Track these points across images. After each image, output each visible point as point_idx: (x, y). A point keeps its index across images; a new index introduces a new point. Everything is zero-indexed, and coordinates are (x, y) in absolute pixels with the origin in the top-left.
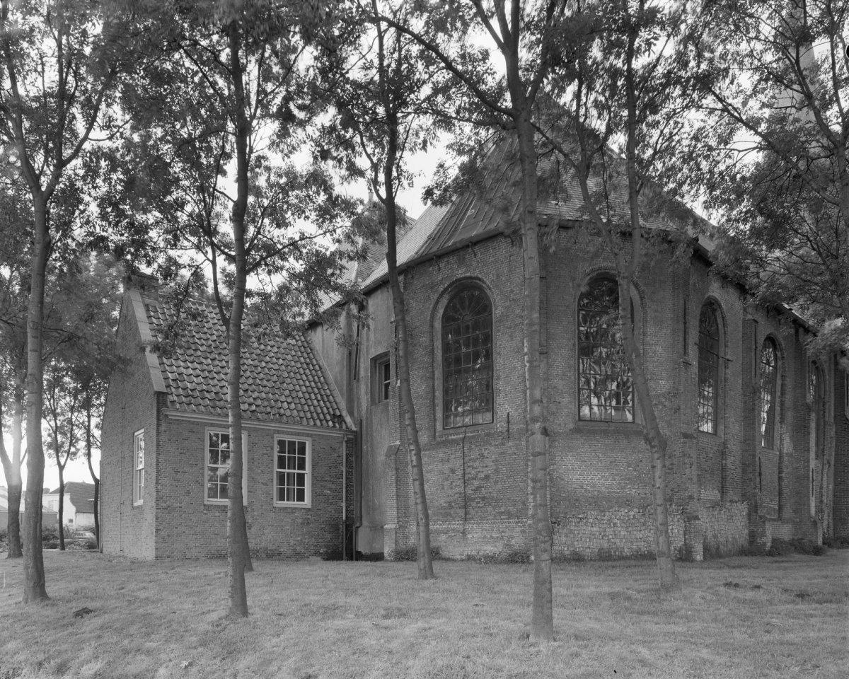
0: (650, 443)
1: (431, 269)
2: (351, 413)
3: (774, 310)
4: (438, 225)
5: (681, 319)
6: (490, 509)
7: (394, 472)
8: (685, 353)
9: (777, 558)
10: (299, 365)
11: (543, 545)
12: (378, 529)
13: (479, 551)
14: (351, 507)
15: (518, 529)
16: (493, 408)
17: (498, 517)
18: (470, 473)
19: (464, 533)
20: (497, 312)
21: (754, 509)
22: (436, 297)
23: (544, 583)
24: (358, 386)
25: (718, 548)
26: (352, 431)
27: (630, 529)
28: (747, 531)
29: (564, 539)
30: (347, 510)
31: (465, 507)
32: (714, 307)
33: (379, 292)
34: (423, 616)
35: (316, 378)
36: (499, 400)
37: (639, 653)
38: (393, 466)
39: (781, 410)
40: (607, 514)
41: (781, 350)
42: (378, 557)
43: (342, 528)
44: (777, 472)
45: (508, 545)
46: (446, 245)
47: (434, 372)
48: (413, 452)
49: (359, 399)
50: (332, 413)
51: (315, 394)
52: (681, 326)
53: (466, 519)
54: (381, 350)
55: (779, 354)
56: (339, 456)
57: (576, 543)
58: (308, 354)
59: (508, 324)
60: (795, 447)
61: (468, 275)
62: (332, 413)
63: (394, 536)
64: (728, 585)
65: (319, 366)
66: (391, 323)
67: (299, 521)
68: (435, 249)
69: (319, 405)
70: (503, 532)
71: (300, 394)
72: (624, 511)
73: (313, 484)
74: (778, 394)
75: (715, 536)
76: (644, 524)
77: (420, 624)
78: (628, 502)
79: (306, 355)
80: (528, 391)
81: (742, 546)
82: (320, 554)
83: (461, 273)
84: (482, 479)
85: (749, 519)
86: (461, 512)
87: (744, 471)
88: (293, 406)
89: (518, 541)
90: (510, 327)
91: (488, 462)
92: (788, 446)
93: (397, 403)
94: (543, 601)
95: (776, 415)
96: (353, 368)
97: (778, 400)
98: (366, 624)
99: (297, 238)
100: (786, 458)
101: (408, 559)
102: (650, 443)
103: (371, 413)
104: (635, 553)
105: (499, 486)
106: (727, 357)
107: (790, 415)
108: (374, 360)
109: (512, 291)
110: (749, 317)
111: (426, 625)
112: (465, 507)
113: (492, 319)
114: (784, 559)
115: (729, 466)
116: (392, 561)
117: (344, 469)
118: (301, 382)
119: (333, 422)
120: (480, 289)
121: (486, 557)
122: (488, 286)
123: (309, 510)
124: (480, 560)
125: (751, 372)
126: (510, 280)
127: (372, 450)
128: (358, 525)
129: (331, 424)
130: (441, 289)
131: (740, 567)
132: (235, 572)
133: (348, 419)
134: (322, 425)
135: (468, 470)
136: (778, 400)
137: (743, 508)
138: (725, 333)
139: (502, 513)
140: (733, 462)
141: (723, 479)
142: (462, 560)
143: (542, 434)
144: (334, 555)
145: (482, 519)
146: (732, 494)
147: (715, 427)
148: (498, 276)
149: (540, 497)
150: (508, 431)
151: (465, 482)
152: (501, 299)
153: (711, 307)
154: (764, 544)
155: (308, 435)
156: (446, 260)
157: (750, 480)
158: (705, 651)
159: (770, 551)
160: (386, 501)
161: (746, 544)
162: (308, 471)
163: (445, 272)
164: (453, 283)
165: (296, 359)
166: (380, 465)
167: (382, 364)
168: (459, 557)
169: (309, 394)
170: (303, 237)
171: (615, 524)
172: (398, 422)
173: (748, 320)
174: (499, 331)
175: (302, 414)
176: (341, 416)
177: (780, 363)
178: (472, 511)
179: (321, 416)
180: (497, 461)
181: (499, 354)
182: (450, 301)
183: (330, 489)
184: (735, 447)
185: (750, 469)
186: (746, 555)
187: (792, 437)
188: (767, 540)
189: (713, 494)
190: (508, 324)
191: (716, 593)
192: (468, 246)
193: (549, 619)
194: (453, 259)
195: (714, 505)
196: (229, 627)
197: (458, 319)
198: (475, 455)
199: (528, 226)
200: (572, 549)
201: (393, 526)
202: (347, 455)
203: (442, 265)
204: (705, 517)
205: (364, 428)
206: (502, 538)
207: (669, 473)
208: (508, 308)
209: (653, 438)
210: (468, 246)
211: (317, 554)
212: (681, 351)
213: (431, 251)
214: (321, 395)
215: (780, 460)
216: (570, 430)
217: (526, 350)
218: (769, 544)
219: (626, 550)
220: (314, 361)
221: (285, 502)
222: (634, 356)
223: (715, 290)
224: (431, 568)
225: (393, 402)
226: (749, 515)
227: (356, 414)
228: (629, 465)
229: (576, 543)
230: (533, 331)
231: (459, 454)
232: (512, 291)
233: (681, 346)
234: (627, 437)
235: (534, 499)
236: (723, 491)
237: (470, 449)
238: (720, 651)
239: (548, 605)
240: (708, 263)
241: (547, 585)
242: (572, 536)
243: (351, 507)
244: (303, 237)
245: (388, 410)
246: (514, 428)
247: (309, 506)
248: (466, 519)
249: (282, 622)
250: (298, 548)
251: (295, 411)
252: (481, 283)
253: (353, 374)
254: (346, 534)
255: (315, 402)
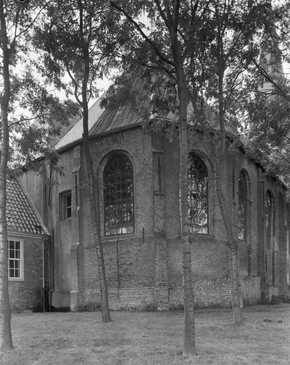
0: (230, 247)
1: (97, 143)
2: (46, 225)
3: (274, 179)
4: (99, 118)
5: (232, 180)
6: (133, 281)
7: (76, 260)
8: (234, 198)
9: (275, 306)
10: (13, 195)
11: (190, 303)
12: (66, 293)
13: (127, 305)
14: (48, 280)
15: (149, 293)
16: (134, 224)
17: (138, 286)
18: (121, 261)
19: (118, 295)
20: (136, 170)
21: (263, 280)
22: (100, 160)
23: (190, 323)
24: (51, 210)
25: (248, 301)
26: (47, 235)
27: (208, 291)
28: (260, 292)
29: (175, 298)
30: (45, 282)
31: (119, 280)
32: (245, 174)
33: (64, 154)
34: (117, 344)
35: (24, 203)
36: (138, 220)
37: (242, 359)
38: (75, 256)
39: (274, 228)
40: (196, 284)
41: (273, 197)
42: (66, 310)
43: (43, 293)
44: (272, 261)
45: (144, 302)
46: (106, 131)
47: (99, 203)
48: (99, 250)
49: (51, 217)
50: (35, 224)
51: (24, 213)
52: (232, 183)
53: (119, 287)
54: (65, 189)
55: (272, 200)
56: (40, 250)
57: (181, 300)
58: (18, 188)
59: (143, 178)
60: (280, 248)
61: (119, 148)
62: (35, 224)
63: (76, 298)
64: (265, 321)
65: (25, 196)
66: (73, 173)
67: (17, 289)
68: (99, 132)
69: (27, 220)
70: (141, 294)
71: (16, 213)
72: (205, 282)
73: (25, 267)
74: (272, 220)
75: (247, 295)
76: (215, 289)
77: (117, 349)
78: (206, 277)
79: (17, 190)
80: (181, 219)
81: (258, 300)
82: (30, 309)
83: (115, 147)
84: (128, 265)
85: (261, 286)
86: (116, 283)
87: (258, 261)
88: (12, 220)
89: (149, 300)
90: (144, 180)
91: (132, 255)
92: (276, 248)
93: (77, 220)
94: (190, 333)
95: (271, 231)
96: (50, 197)
97: (272, 224)
98: (87, 350)
99: (19, 119)
100: (276, 254)
101: (86, 311)
102: (230, 247)
103: (60, 225)
104: (211, 305)
105: (138, 268)
106: (251, 201)
107: (277, 231)
108: (61, 194)
109: (145, 160)
110: (261, 180)
111: (121, 349)
112: (119, 280)
113: (133, 175)
114: (278, 306)
115: (252, 258)
116: (76, 312)
117: (43, 258)
118: (15, 206)
119: (36, 230)
120: (126, 157)
121: (132, 308)
122: (131, 156)
123: (23, 282)
124: (129, 310)
125: (261, 209)
126: (141, 154)
127: (61, 247)
128: (52, 291)
129: (35, 231)
130: (103, 155)
131: (262, 311)
132: (5, 322)
133: (45, 228)
134: (30, 231)
135: (120, 260)
136: (272, 224)
137: (258, 280)
138: (250, 188)
139: (140, 284)
140: (253, 255)
141: (249, 265)
142: (118, 310)
143: (189, 242)
144: (38, 309)
145: (129, 287)
146: (254, 273)
147: (245, 236)
148: (137, 151)
149: (188, 276)
150: (143, 238)
151: (118, 266)
152: (139, 164)
153: (244, 173)
154: (269, 298)
155: (21, 238)
156: (106, 139)
157: (262, 265)
158: (273, 357)
159: (271, 302)
160: (70, 277)
161: (260, 298)
162: (21, 259)
163: (105, 146)
164: (110, 152)
165: (11, 191)
166: (65, 256)
167: (66, 197)
168: (115, 309)
169: (21, 213)
170: (22, 119)
171: (200, 289)
172: (78, 231)
173: (260, 181)
174: (137, 181)
175: (17, 225)
176: (40, 227)
177: (273, 204)
178: (122, 282)
179: (29, 226)
180: (137, 254)
181: (138, 194)
182: (108, 163)
183: (35, 270)
184: (254, 248)
185: (261, 260)
186: (261, 304)
187: (278, 243)
188: (270, 296)
189: (245, 273)
190: (143, 178)
191: (262, 325)
192: (118, 132)
193: (193, 343)
194: (110, 139)
195: (246, 279)
196: (5, 355)
197: (113, 173)
198: (124, 250)
199: (183, 127)
200: (178, 303)
201: (76, 291)
202: (45, 250)
203: (103, 142)
204: (243, 285)
205: (55, 234)
206: (140, 298)
207: (226, 262)
208: (142, 169)
209: (232, 244)
210: (118, 132)
211: (28, 308)
212: (232, 196)
213: (97, 133)
214: (28, 214)
215: (273, 254)
216: (177, 238)
217: (180, 195)
218: (271, 299)
219: (206, 303)
220: (22, 193)
221: (14, 278)
222: (222, 199)
223: (246, 166)
224: (109, 315)
225: (74, 219)
226: (261, 283)
227: (49, 226)
228: (206, 257)
229: (181, 300)
230: (185, 185)
231: (115, 250)
232: (145, 160)
233: (231, 194)
234: (205, 242)
235: (185, 278)
236: (249, 270)
237: (121, 248)
238: (281, 356)
239: (193, 336)
240: (244, 153)
241: (192, 325)
242: (179, 296)
243: (48, 280)
244: (22, 119)
245: (71, 224)
246: (147, 236)
247: (23, 280)
248: (119, 287)
249: (36, 351)
250: (17, 305)
251: (13, 223)
252: (126, 154)
253: (47, 202)
254: (45, 296)
255: (25, 217)
